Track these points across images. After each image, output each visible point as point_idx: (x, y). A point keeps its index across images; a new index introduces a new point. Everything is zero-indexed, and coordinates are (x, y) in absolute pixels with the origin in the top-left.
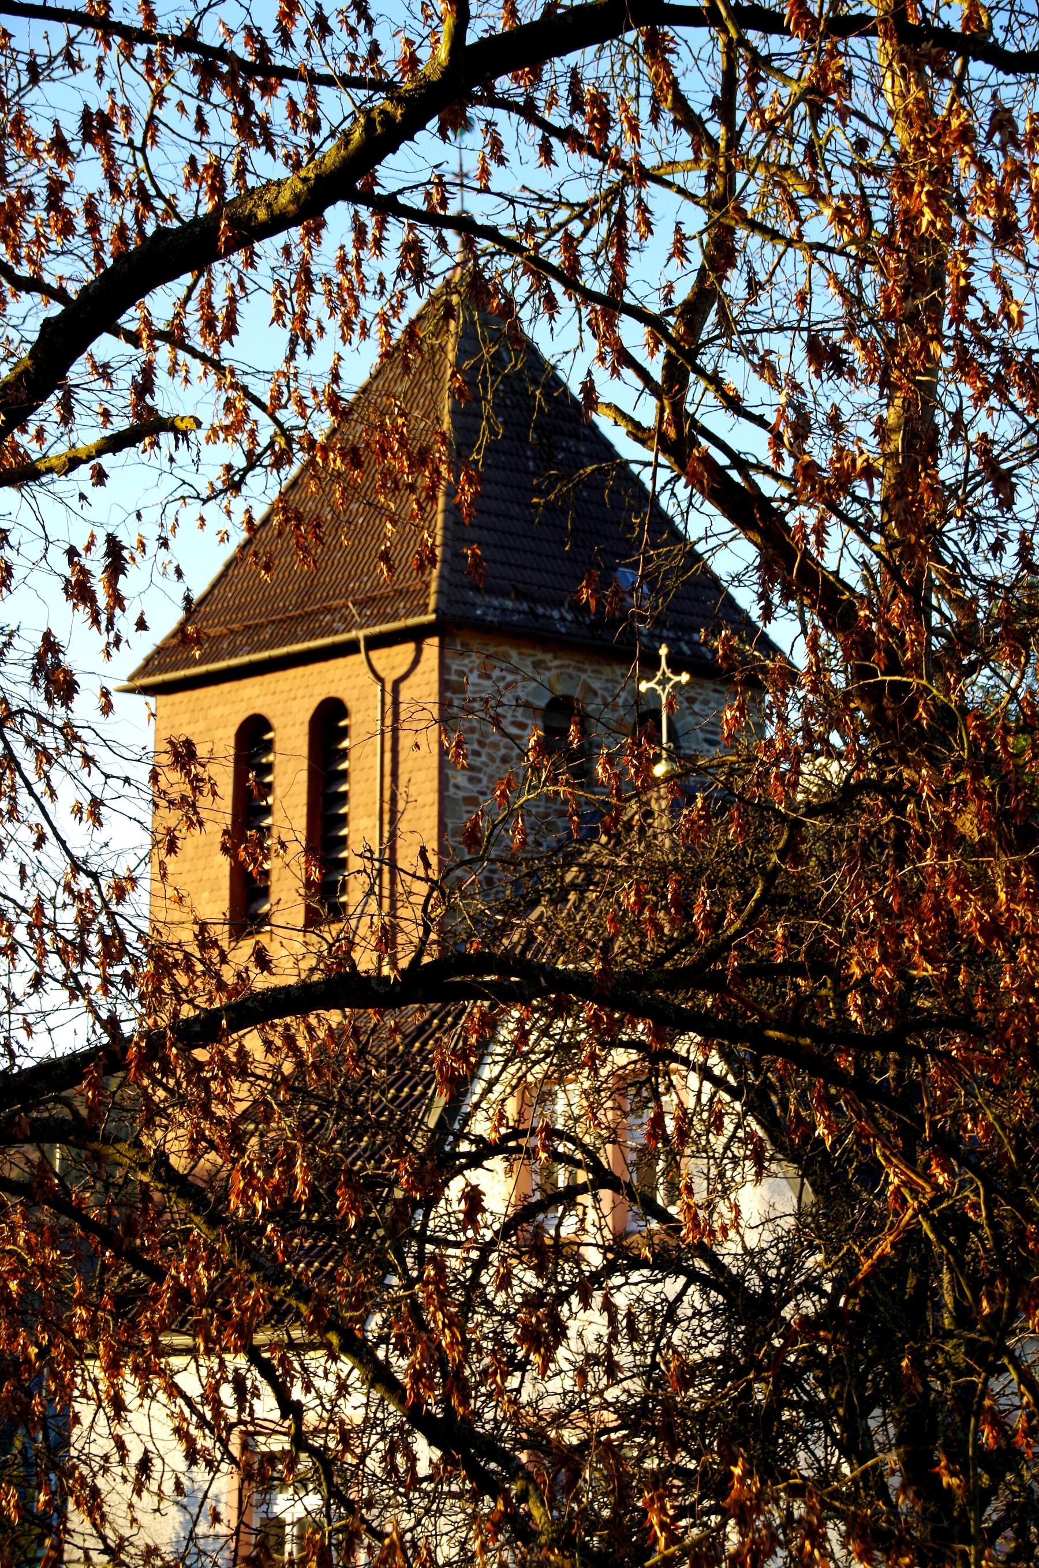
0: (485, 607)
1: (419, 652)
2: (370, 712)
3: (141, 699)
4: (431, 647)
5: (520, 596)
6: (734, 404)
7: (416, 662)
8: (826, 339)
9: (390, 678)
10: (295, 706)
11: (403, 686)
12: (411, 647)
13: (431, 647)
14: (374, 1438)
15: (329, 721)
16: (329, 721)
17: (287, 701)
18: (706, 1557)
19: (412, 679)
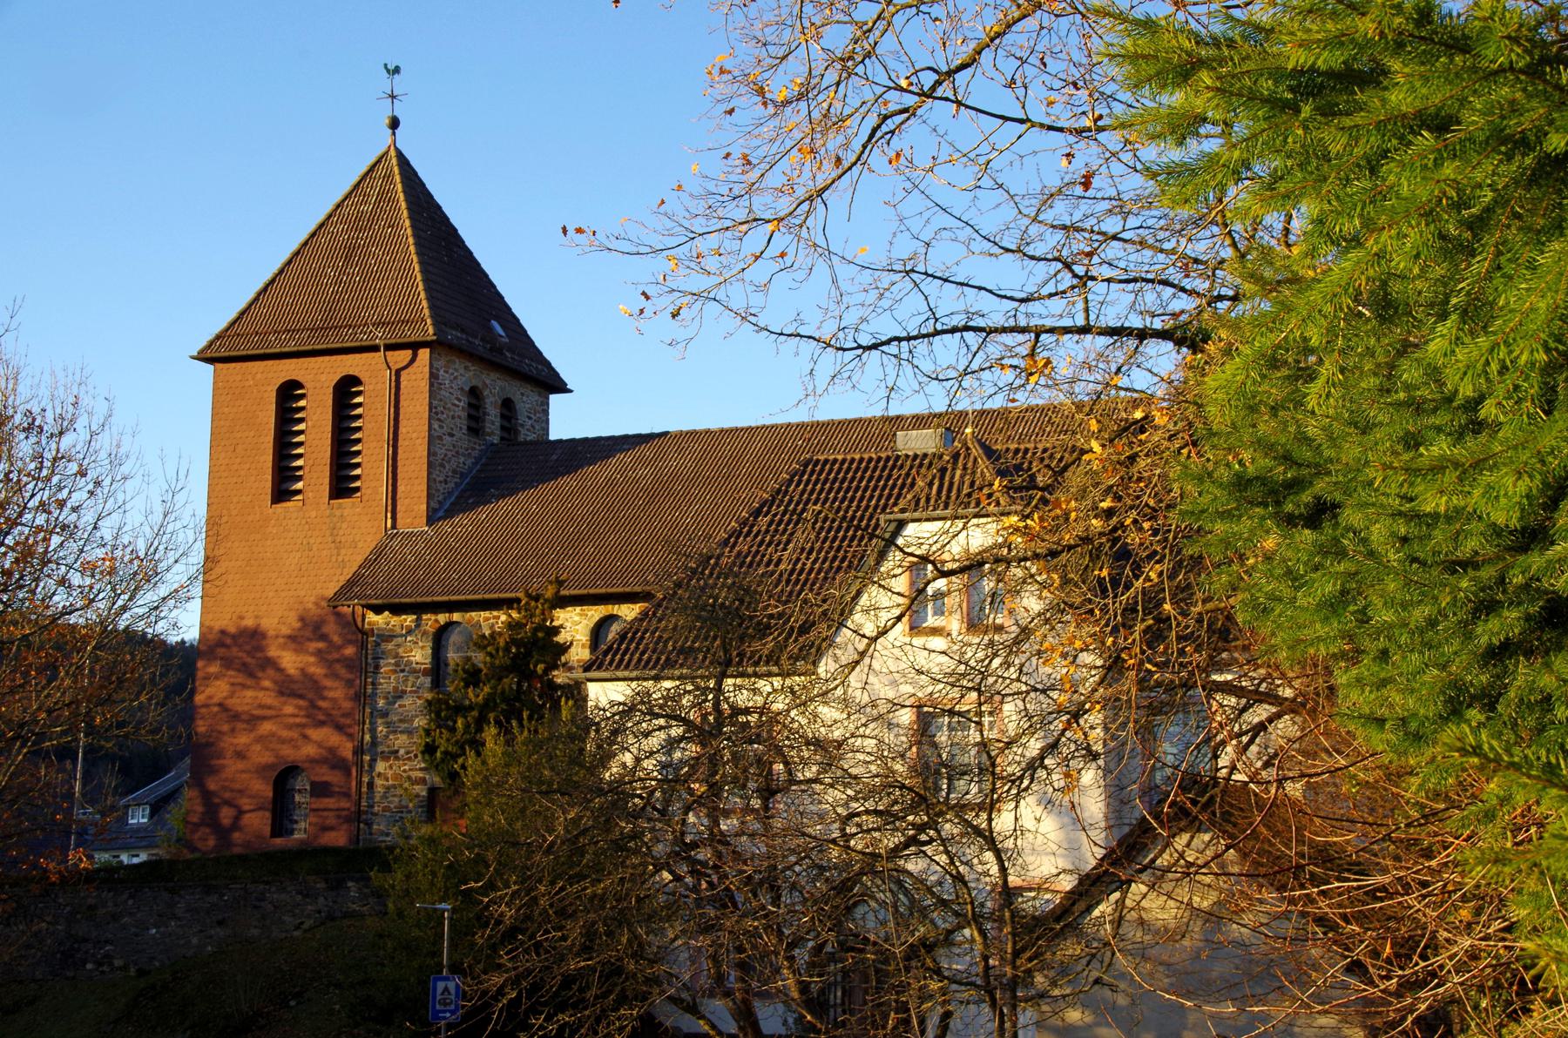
0: (452, 335)
1: (415, 356)
2: (379, 386)
3: (210, 368)
4: (424, 354)
5: (463, 331)
6: (1319, 775)
7: (413, 361)
8: (473, 677)
9: (394, 368)
10: (323, 378)
11: (404, 374)
12: (410, 352)
13: (424, 354)
14: (125, 896)
15: (346, 389)
16: (346, 389)
17: (318, 377)
18: (875, 1036)
19: (409, 370)
